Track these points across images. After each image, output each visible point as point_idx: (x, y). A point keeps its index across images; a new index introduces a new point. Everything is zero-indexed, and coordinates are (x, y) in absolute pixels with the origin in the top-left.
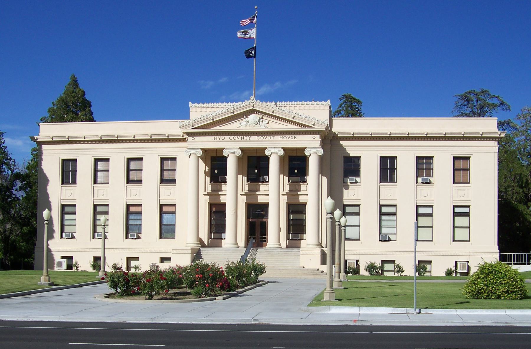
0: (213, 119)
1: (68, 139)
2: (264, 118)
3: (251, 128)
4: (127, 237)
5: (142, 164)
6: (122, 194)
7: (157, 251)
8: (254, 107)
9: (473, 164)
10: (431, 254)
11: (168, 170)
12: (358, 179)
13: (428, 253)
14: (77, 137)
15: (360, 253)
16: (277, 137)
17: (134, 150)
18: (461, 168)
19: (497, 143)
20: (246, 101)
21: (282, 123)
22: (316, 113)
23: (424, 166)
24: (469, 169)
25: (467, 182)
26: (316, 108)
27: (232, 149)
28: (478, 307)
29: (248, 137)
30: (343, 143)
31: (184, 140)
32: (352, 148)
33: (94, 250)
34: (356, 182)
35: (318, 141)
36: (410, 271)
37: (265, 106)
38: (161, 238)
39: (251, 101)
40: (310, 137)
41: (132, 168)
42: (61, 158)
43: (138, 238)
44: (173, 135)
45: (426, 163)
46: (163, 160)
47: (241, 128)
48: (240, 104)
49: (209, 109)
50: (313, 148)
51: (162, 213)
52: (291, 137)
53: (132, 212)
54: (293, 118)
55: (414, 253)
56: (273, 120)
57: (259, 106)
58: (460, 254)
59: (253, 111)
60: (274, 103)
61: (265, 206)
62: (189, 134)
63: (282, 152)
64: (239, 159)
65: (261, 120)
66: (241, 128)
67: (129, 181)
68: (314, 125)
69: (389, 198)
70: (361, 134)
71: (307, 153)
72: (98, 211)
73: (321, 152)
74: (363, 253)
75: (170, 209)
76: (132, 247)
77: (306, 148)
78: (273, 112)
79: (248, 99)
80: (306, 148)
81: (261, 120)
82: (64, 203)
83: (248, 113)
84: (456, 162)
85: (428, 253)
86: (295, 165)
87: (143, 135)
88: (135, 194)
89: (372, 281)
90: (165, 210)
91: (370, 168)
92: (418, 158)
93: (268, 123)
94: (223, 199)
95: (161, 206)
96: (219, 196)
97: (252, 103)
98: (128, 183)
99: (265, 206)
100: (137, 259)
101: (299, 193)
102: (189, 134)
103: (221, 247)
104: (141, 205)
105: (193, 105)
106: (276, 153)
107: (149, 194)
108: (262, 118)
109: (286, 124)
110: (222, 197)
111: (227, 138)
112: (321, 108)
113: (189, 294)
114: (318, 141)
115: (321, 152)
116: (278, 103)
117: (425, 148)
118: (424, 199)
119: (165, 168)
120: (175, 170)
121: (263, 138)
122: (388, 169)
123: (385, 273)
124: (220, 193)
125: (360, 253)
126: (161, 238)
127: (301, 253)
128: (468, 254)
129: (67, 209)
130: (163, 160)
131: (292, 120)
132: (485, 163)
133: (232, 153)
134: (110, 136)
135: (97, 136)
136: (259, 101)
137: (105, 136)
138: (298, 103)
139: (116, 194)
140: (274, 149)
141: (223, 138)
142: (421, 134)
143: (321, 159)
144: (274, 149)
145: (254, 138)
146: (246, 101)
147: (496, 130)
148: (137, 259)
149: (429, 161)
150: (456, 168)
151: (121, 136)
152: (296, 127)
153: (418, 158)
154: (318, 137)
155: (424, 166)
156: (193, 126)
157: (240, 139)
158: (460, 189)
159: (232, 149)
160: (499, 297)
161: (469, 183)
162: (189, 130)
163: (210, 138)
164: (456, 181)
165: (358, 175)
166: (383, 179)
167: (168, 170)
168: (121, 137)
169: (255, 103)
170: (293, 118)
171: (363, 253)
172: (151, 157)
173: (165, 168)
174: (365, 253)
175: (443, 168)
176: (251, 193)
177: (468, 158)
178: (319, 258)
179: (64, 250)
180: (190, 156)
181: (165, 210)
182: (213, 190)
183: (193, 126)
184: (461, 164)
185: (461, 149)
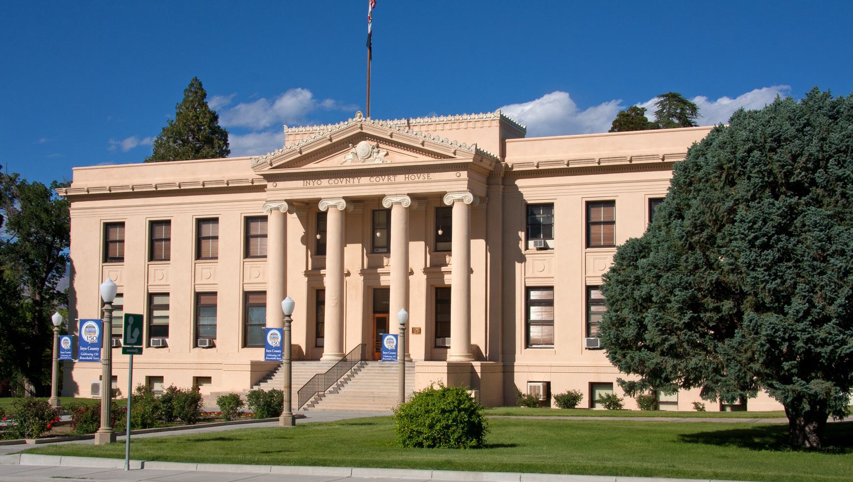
1: (133, 189)
2: (380, 145)
3: (361, 163)
4: (196, 345)
6: (188, 276)
8: (361, 128)
11: (599, 223)
15: (553, 369)
16: (400, 178)
20: (342, 123)
27: (332, 197)
28: (578, 457)
29: (356, 180)
30: (519, 183)
31: (262, 189)
32: (532, 191)
33: (146, 366)
34: (546, 248)
35: (464, 180)
37: (379, 126)
39: (357, 119)
40: (452, 175)
41: (253, 232)
43: (212, 346)
47: (345, 164)
48: (343, 125)
50: (457, 192)
52: (423, 177)
53: (204, 303)
55: (128, 366)
57: (371, 126)
60: (404, 121)
62: (269, 178)
64: (410, 213)
65: (376, 150)
66: (345, 164)
68: (455, 153)
70: (552, 165)
72: (532, 298)
74: (557, 369)
76: (201, 360)
79: (353, 117)
82: (248, 288)
87: (217, 182)
89: (669, 419)
93: (387, 154)
94: (384, 281)
97: (358, 122)
100: (208, 380)
102: (269, 178)
104: (167, 294)
105: (290, 130)
108: (378, 147)
109: (415, 154)
110: (382, 278)
111: (325, 182)
112: (487, 124)
114: (464, 180)
116: (412, 121)
119: (253, 233)
120: (613, 223)
123: (662, 407)
124: (380, 270)
125: (553, 369)
128: (548, 369)
129: (157, 301)
131: (421, 146)
135: (150, 185)
136: (369, 119)
140: (396, 195)
141: (319, 182)
143: (472, 210)
144: (396, 195)
145: (365, 180)
146: (350, 120)
148: (208, 380)
151: (115, 187)
154: (464, 174)
155: (204, 231)
156: (271, 164)
158: (204, 267)
159: (332, 197)
162: (267, 170)
163: (300, 183)
165: (550, 236)
167: (599, 223)
168: (115, 189)
169: (363, 123)
170: (423, 144)
171: (557, 369)
173: (253, 233)
174: (562, 369)
181: (253, 302)
183: (271, 164)
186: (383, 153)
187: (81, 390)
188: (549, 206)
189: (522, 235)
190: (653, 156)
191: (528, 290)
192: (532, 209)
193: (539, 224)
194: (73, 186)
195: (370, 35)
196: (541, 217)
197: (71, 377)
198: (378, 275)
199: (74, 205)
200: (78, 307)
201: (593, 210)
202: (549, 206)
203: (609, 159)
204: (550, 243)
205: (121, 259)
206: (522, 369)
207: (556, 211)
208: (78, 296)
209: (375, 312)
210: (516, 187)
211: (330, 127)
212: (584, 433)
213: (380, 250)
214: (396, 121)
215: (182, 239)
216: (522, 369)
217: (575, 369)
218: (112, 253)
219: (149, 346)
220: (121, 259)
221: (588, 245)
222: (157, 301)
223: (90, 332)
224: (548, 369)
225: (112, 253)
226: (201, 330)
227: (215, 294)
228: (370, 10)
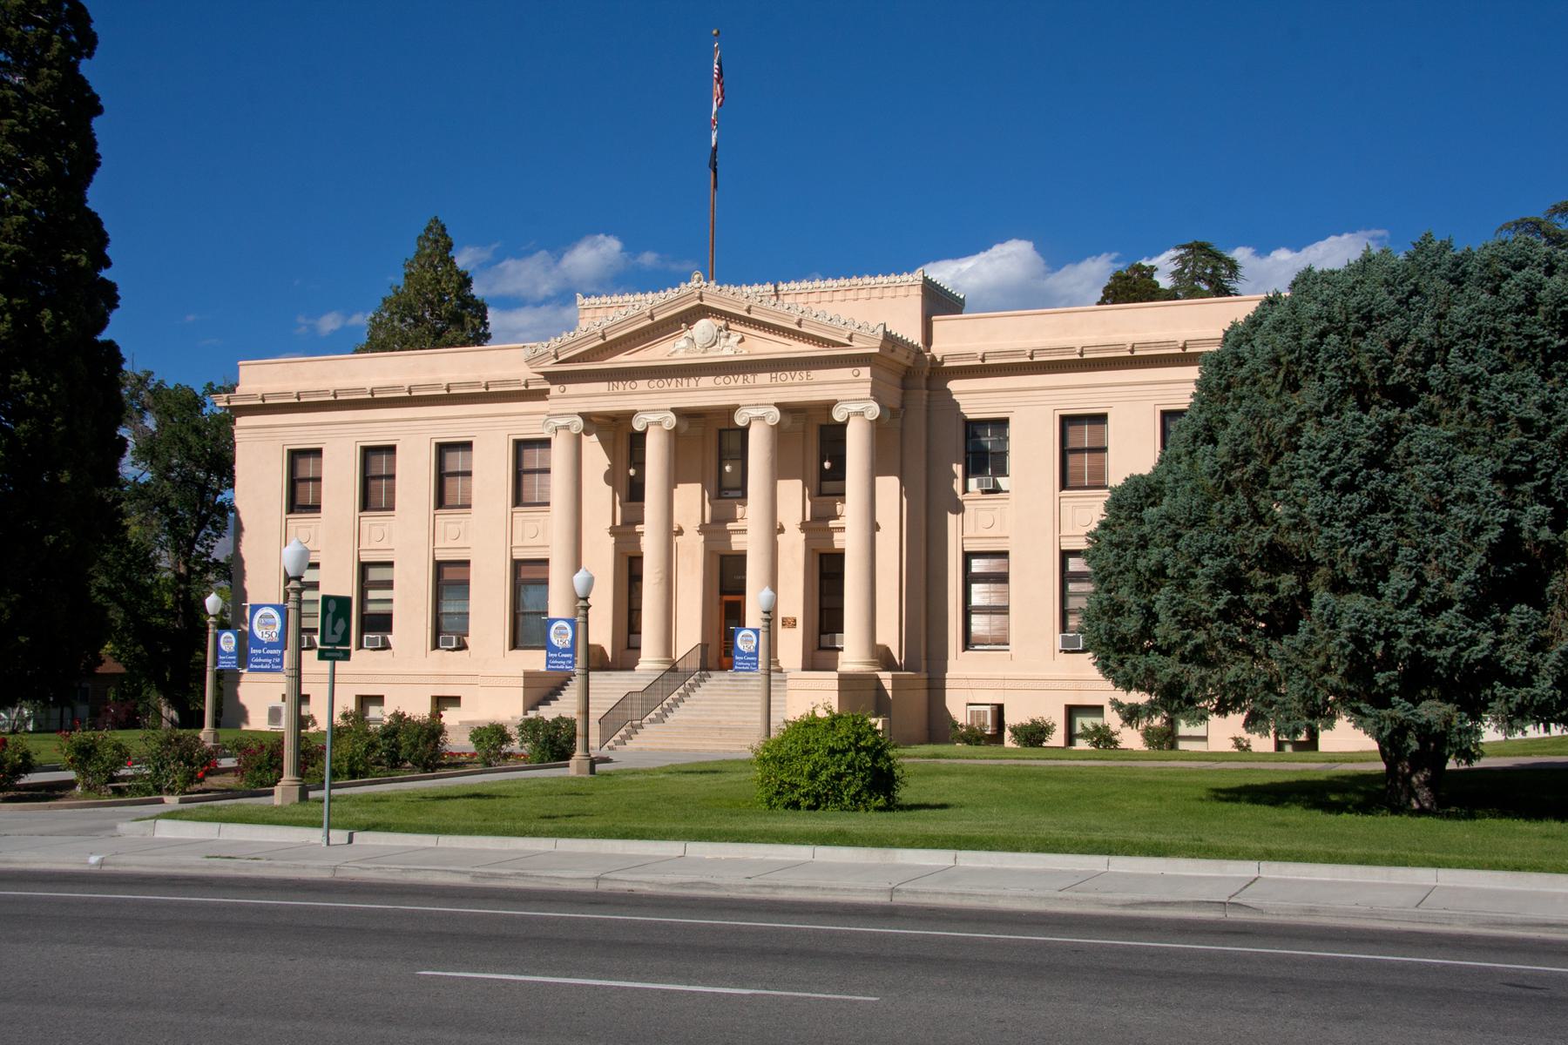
0: (603, 337)
2: (732, 326)
4: (436, 646)
5: (320, 465)
6: (424, 535)
8: (701, 298)
11: (1082, 451)
12: (1002, 481)
15: (1008, 684)
16: (763, 378)
20: (683, 285)
21: (777, 338)
27: (654, 409)
29: (692, 381)
30: (954, 385)
31: (541, 395)
32: (974, 399)
34: (997, 490)
37: (729, 295)
39: (694, 283)
40: (845, 373)
42: (1058, 413)
43: (462, 646)
44: (1146, 345)
46: (1067, 421)
48: (671, 294)
49: (600, 313)
50: (854, 400)
52: (799, 376)
54: (799, 324)
56: (752, 331)
60: (769, 287)
65: (724, 333)
68: (850, 338)
72: (974, 570)
77: (738, 406)
78: (749, 311)
81: (724, 333)
93: (742, 340)
94: (737, 542)
96: (728, 534)
99: (741, 558)
100: (455, 701)
105: (587, 301)
108: (727, 328)
109: (791, 342)
110: (734, 538)
111: (642, 384)
112: (902, 291)
113: (71, 785)
115: (873, 410)
116: (782, 287)
120: (1104, 450)
121: (730, 380)
123: (1182, 745)
124: (730, 526)
125: (1008, 684)
127: (790, 684)
128: (1000, 684)
130: (1067, 421)
133: (655, 423)
136: (712, 283)
138: (842, 281)
140: (757, 406)
142: (1169, 347)
143: (878, 430)
144: (757, 406)
145: (706, 381)
146: (683, 285)
148: (455, 701)
150: (1071, 445)
152: (811, 347)
154: (865, 372)
156: (556, 356)
157: (740, 382)
159: (654, 409)
160: (795, 805)
162: (550, 366)
163: (602, 387)
165: (1002, 471)
166: (366, 504)
167: (1082, 451)
169: (704, 289)
170: (799, 324)
176: (716, 527)
181: (527, 577)
182: (713, 520)
183: (556, 356)
187: (252, 717)
189: (958, 469)
190: (1168, 343)
192: (973, 428)
195: (715, 149)
196: (988, 440)
197: (236, 696)
199: (241, 421)
201: (1072, 430)
208: (247, 567)
209: (723, 592)
212: (1057, 787)
213: (731, 494)
214: (756, 288)
218: (301, 495)
219: (360, 646)
224: (1000, 684)
225: (301, 495)
226: (444, 621)
227: (467, 563)
228: (715, 108)
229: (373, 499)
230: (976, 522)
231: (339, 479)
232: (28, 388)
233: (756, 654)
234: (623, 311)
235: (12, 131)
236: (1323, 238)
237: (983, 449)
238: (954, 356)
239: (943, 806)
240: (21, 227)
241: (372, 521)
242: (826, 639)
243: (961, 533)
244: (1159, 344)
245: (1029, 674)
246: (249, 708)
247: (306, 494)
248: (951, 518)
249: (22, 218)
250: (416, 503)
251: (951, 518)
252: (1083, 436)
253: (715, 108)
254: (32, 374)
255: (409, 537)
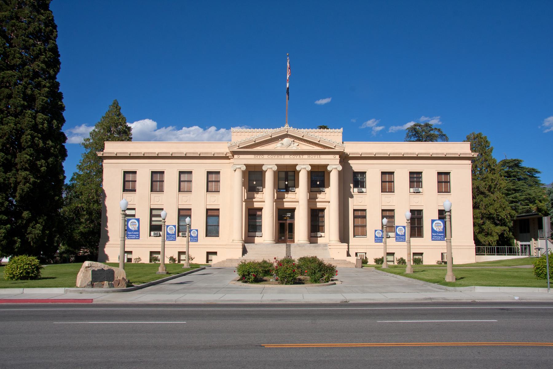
7: (205, 246)
9: (222, 177)
10: (422, 247)
11: (129, 181)
13: (420, 247)
14: (137, 153)
15: (368, 247)
16: (306, 157)
17: (158, 165)
18: (444, 179)
19: (470, 161)
22: (333, 137)
23: (415, 179)
24: (449, 182)
25: (161, 191)
26: (332, 134)
29: (282, 156)
30: (350, 162)
32: (356, 166)
36: (146, 260)
38: (206, 236)
39: (286, 127)
45: (416, 178)
48: (278, 130)
49: (254, 134)
50: (334, 165)
51: (151, 216)
57: (292, 131)
58: (359, 247)
59: (287, 136)
61: (292, 210)
63: (244, 168)
67: (124, 190)
69: (213, 203)
71: (264, 168)
73: (340, 168)
75: (132, 212)
77: (297, 165)
79: (283, 126)
80: (297, 165)
82: (209, 207)
83: (282, 137)
84: (210, 176)
85: (420, 247)
86: (318, 179)
87: (193, 153)
88: (157, 200)
90: (212, 215)
91: (373, 180)
92: (411, 173)
95: (151, 210)
97: (286, 129)
98: (124, 191)
100: (215, 253)
101: (254, 200)
102: (234, 153)
103: (254, 243)
106: (305, 168)
107: (198, 201)
111: (266, 156)
117: (416, 165)
118: (409, 204)
121: (295, 157)
122: (387, 182)
125: (368, 247)
126: (206, 236)
132: (462, 177)
134: (166, 153)
135: (141, 153)
137: (161, 153)
139: (402, 202)
140: (303, 166)
144: (303, 166)
145: (287, 157)
147: (470, 151)
148: (215, 253)
149: (418, 176)
151: (175, 153)
153: (411, 173)
155: (415, 179)
158: (387, 196)
159: (270, 165)
161: (450, 192)
162: (236, 149)
163: (252, 156)
164: (209, 189)
167: (212, 181)
171: (370, 247)
172: (199, 171)
175: (430, 180)
176: (248, 200)
177: (392, 173)
178: (240, 251)
179: (209, 246)
180: (235, 171)
181: (212, 215)
182: (248, 198)
184: (387, 177)
185: (444, 166)
186: (296, 144)
187: (110, 258)
188: (364, 173)
189: (352, 185)
190: (413, 154)
191: (354, 210)
192: (356, 174)
193: (358, 181)
194: (105, 151)
195: (288, 88)
196: (359, 177)
197: (104, 252)
198: (253, 202)
199: (105, 161)
200: (108, 215)
201: (127, 175)
202: (364, 173)
203: (394, 154)
204: (364, 190)
205: (134, 190)
206: (352, 247)
207: (368, 175)
208: (107, 209)
209: (279, 220)
210: (349, 164)
211: (271, 129)
212: (493, 272)
213: (282, 190)
214: (306, 130)
215: (171, 181)
216: (352, 247)
217: (432, 247)
218: (128, 186)
219: (178, 236)
220: (134, 190)
221: (152, 191)
222: (154, 212)
223: (438, 226)
224: (365, 247)
225: (128, 186)
226: (181, 227)
227: (218, 210)
228: (288, 76)
229: (154, 188)
230: (356, 201)
231: (143, 181)
232: (52, 146)
233: (404, 235)
234: (262, 134)
235: (44, 60)
236: (144, 119)
237: (359, 180)
238: (353, 154)
239: (462, 278)
240: (47, 92)
241: (155, 195)
242: (252, 234)
243: (354, 203)
244: (411, 153)
245: (422, 244)
246: (109, 255)
247: (130, 186)
248: (350, 199)
249: (47, 89)
250: (176, 189)
251: (350, 199)
252: (130, 177)
253: (288, 76)
254: (52, 142)
255: (169, 201)
